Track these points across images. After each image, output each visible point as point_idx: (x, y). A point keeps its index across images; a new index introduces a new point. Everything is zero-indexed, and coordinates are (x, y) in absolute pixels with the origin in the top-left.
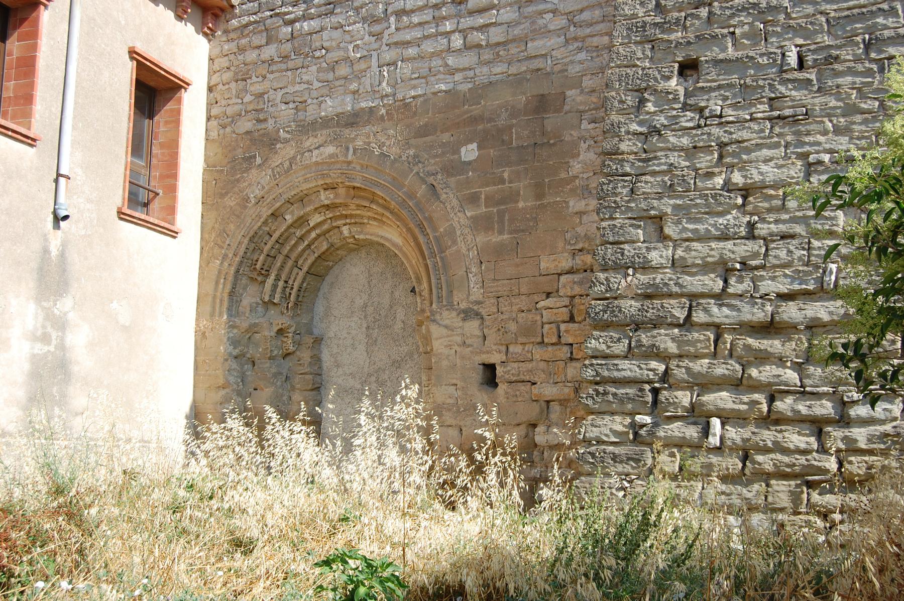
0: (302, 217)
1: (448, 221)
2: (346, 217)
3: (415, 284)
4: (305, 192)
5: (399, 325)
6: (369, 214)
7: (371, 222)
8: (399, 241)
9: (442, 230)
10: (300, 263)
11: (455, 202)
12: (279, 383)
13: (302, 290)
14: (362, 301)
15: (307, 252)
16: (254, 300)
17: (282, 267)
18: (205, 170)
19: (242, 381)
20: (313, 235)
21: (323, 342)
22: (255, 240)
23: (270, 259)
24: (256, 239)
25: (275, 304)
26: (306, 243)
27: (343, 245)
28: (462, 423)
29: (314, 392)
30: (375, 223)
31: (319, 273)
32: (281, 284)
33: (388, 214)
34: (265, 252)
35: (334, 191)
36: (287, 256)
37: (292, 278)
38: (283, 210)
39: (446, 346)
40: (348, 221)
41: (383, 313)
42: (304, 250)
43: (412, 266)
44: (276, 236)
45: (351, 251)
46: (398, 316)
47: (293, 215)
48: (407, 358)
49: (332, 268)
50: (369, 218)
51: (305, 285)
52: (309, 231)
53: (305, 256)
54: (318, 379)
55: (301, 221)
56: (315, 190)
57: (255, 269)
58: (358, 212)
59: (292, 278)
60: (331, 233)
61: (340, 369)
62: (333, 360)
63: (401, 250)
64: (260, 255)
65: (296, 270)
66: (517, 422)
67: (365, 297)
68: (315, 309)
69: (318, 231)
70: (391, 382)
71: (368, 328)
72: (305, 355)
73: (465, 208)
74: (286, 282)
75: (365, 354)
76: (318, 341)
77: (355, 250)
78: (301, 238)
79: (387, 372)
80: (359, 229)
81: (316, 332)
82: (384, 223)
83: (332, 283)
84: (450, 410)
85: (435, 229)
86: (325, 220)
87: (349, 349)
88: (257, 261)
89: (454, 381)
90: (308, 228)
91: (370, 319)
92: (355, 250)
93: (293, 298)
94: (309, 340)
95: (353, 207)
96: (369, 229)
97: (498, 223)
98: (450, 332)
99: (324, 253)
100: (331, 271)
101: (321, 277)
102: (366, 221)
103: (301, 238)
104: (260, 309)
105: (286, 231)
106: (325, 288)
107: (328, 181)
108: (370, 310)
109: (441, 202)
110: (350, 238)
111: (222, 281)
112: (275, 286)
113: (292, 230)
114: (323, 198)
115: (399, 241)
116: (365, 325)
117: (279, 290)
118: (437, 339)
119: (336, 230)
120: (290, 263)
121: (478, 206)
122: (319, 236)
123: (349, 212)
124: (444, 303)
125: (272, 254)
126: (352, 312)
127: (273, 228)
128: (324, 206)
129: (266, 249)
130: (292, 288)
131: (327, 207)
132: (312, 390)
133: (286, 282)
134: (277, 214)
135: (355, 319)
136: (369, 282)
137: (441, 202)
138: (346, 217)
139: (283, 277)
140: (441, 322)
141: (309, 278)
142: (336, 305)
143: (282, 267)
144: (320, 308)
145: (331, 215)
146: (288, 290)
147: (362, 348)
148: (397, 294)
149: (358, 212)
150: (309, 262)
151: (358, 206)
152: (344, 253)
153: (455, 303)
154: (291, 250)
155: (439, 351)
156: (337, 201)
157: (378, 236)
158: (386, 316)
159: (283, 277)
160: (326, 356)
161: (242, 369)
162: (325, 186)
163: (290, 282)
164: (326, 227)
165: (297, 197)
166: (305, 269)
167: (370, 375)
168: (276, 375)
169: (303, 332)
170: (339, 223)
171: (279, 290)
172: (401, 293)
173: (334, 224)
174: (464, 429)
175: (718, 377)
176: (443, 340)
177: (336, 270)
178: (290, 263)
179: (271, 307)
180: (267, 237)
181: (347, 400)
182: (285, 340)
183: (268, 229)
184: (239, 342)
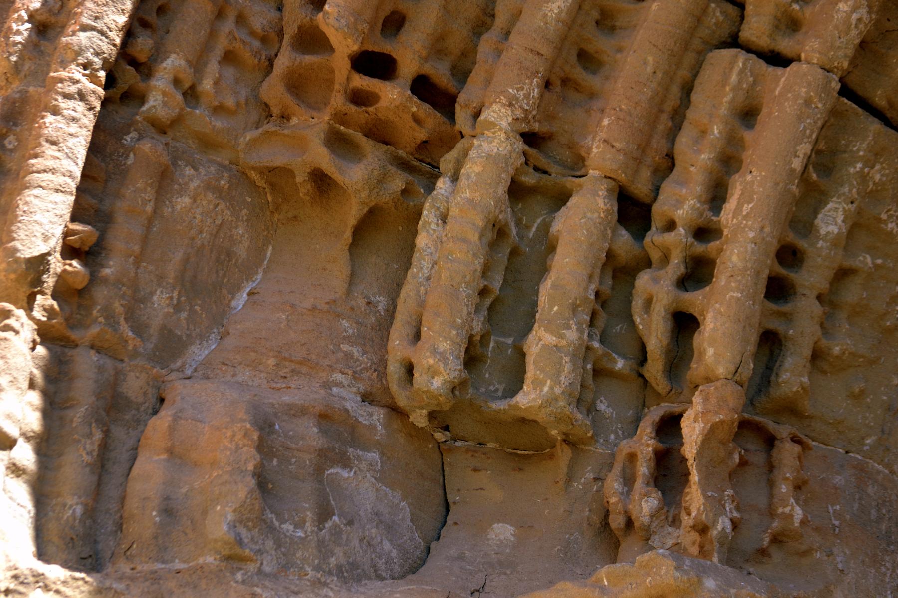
13: (811, 279)
32: (582, 222)
37: (697, 158)
51: (831, 221)
59: (697, 158)
74: (633, 212)
104: (363, 485)
117: (568, 275)
130: (698, 273)
139: (604, 144)
146: (656, 290)
159: (604, 144)
163: (681, 202)
171: (568, 275)
179: (481, 486)
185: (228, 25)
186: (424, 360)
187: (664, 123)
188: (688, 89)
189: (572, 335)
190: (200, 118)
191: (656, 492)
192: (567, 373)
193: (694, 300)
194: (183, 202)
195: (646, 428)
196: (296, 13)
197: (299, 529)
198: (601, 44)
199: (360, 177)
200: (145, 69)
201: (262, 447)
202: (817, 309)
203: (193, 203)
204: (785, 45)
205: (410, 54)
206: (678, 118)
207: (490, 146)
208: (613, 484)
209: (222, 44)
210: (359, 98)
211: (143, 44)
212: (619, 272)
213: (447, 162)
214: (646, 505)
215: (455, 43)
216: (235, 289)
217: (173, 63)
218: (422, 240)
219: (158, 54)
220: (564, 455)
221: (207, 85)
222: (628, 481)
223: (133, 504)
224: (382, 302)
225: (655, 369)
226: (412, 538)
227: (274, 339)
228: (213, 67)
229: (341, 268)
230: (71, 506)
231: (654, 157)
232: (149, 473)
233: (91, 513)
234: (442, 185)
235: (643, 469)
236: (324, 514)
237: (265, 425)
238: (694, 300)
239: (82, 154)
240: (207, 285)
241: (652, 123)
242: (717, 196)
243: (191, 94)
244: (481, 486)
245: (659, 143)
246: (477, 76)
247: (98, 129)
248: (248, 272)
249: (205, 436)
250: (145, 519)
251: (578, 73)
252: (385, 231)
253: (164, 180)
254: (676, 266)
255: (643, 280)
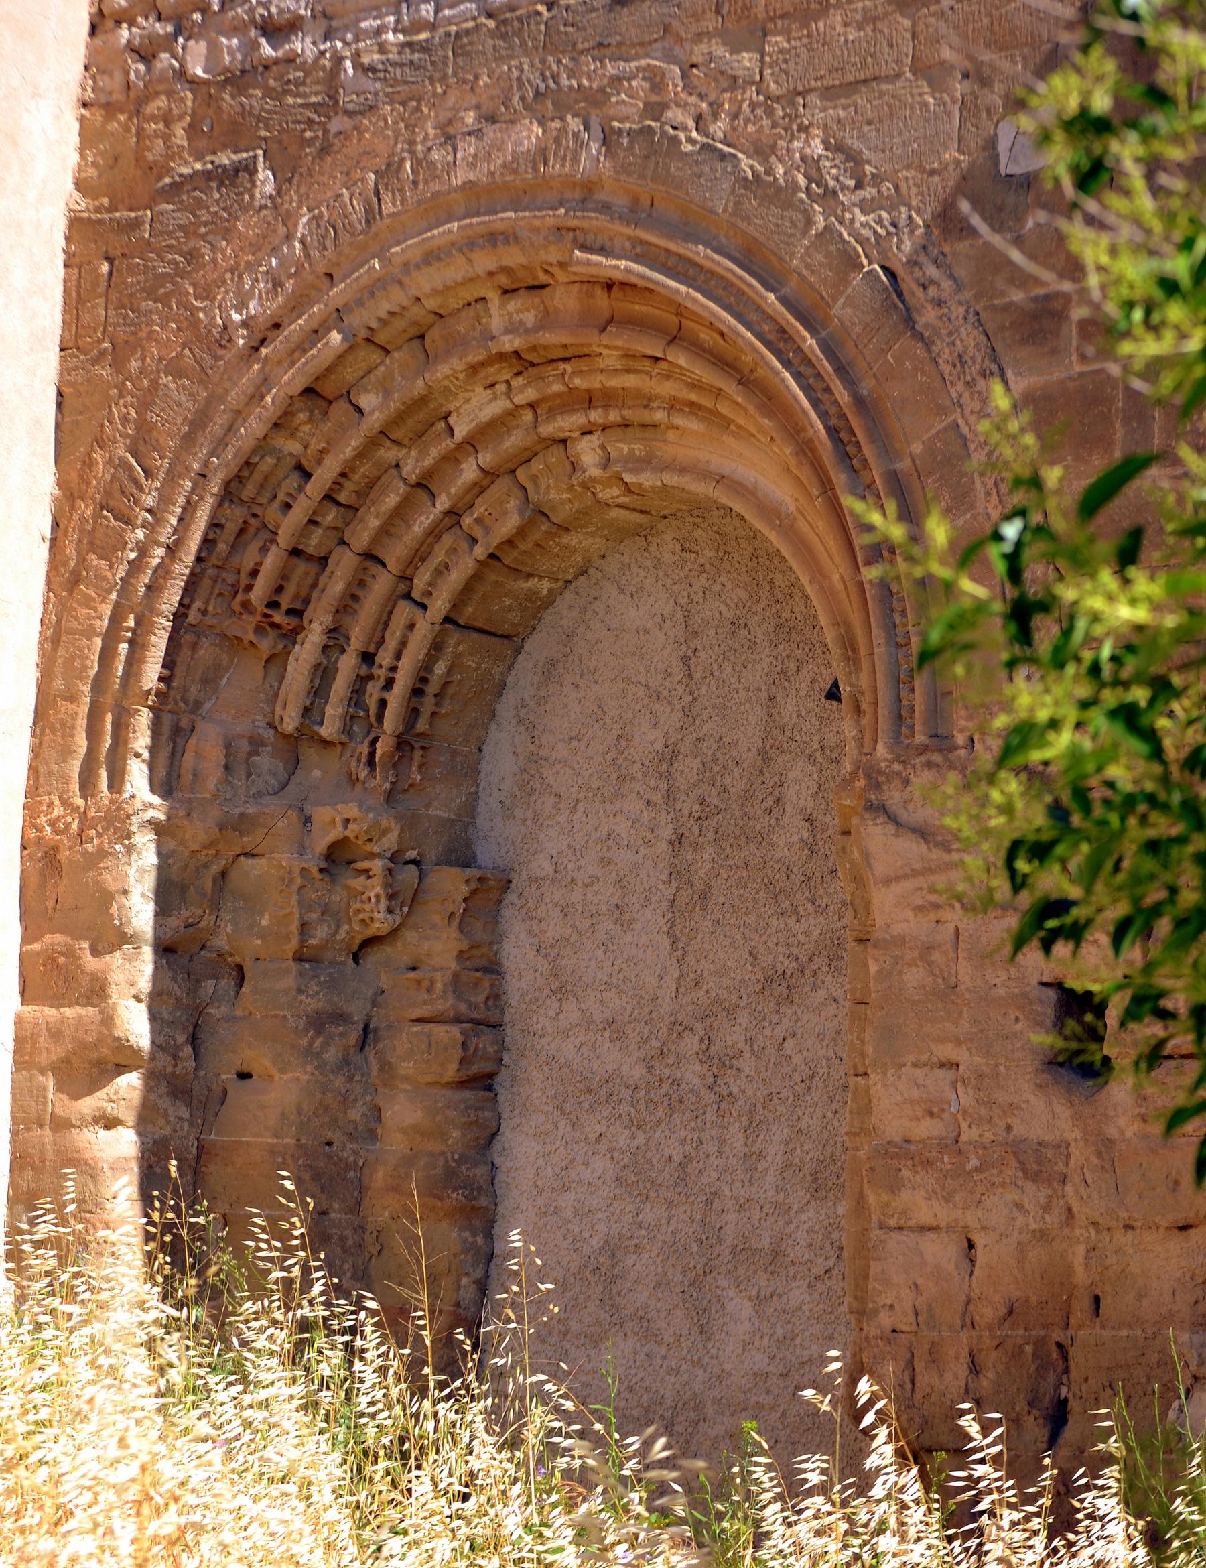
0: (423, 400)
1: (942, 411)
2: (589, 400)
3: (838, 670)
4: (431, 304)
5: (793, 831)
6: (668, 389)
7: (678, 421)
8: (783, 493)
9: (917, 448)
10: (421, 581)
11: (969, 337)
12: (332, 1054)
13: (431, 689)
14: (657, 735)
15: (447, 540)
16: (242, 727)
17: (349, 603)
18: (76, 224)
19: (194, 1040)
20: (469, 472)
21: (511, 897)
22: (244, 496)
23: (301, 567)
24: (248, 491)
25: (325, 744)
26: (443, 503)
27: (584, 512)
28: (971, 1218)
29: (468, 1094)
30: (694, 425)
31: (492, 628)
32: (347, 664)
33: (731, 388)
34: (284, 539)
35: (536, 298)
36: (371, 557)
37: (391, 644)
38: (349, 374)
39: (919, 909)
40: (595, 416)
41: (735, 782)
42: (434, 534)
43: (828, 593)
44: (324, 475)
45: (622, 534)
46: (790, 794)
47: (387, 393)
48: (819, 962)
49: (549, 601)
50: (673, 406)
51: (440, 668)
52: (452, 459)
53: (439, 555)
54: (485, 1042)
55: (422, 417)
56: (468, 294)
57: (246, 605)
58: (631, 381)
59: (391, 644)
60: (537, 466)
61: (570, 1006)
62: (544, 965)
63: (788, 529)
64: (264, 550)
65: (404, 611)
66: (1181, 1217)
67: (671, 718)
68: (484, 767)
69: (486, 458)
70: (757, 1056)
71: (678, 840)
72: (439, 946)
73: (1005, 360)
74: (368, 658)
75: (666, 943)
76: (490, 892)
77: (635, 532)
78: (424, 486)
79: (743, 1019)
80: (638, 448)
81: (486, 854)
82: (725, 424)
83: (552, 663)
84: (928, 1163)
85: (887, 447)
86: (513, 413)
87: (606, 926)
88: (254, 573)
89: (947, 1051)
90: (448, 444)
91: (687, 805)
92: (635, 532)
93: (391, 721)
94: (450, 885)
95: (611, 359)
96: (672, 448)
97: (1126, 421)
98: (936, 854)
99: (510, 542)
100: (548, 616)
101: (507, 639)
102: (659, 416)
103: (424, 486)
104: (266, 761)
105: (361, 455)
106: (523, 677)
107: (513, 257)
108: (687, 769)
109: (920, 337)
110: (607, 483)
111: (123, 647)
112: (323, 674)
113: (389, 454)
114: (496, 323)
115: (783, 493)
116: (667, 832)
117: (341, 686)
118: (888, 882)
119: (555, 456)
120: (381, 584)
121: (1054, 352)
122: (489, 475)
123: (596, 382)
124: (920, 739)
125: (314, 542)
126: (622, 778)
127: (316, 444)
128: (502, 356)
129: (289, 526)
130: (389, 684)
131: (520, 362)
132: (463, 1084)
133: (368, 658)
134: (328, 389)
135: (633, 805)
136: (685, 660)
137: (920, 337)
138: (589, 400)
139: (357, 638)
140: (903, 816)
141: (456, 642)
142: (562, 751)
143: (349, 603)
144: (501, 760)
145: (531, 394)
146: (373, 691)
147: (652, 919)
148: (788, 708)
149: (631, 381)
150: (455, 578)
151: (628, 356)
152: (594, 544)
153: (960, 739)
154: (385, 531)
155: (897, 929)
156: (550, 338)
157: (705, 475)
158: (747, 797)
159: (357, 638)
160: (518, 953)
161: (193, 992)
162: (503, 280)
163: (385, 658)
164: (514, 441)
165: (399, 324)
166: (439, 605)
167: (679, 1028)
168: (319, 1022)
169: (431, 855)
170: (566, 424)
171: (341, 686)
172: (799, 703)
173: (547, 430)
174: (979, 1240)
175: (125, 764)
176: (909, 884)
177: (565, 610)
178: (381, 584)
179: (310, 754)
180: (294, 480)
181: (593, 1128)
182: (359, 883)
183: (294, 447)
184: (184, 889)
185: (219, 585)
186: (286, 719)
187: (381, 626)
188: (391, 613)
189: (340, 710)
190: (209, 620)
191: (1123, 142)
192: (338, 724)
193: (386, 695)
194: (201, 652)
195: (366, 744)
196: (9, 1524)
197: (239, 782)
198: (360, 593)
199: (266, 645)
200: (188, 607)
201: (227, 756)
202: (433, 700)
203: (207, 651)
204: (426, 601)
205: (285, 601)
206: (386, 624)
207: (314, 636)
208: (354, 764)
209: (217, 591)
210: (266, 616)
211: (186, 601)
212: (361, 682)
213: (300, 638)
214: (363, 773)
215: (304, 592)
216: (221, 678)
217: (198, 604)
218: (289, 668)
219: (192, 601)
220: (339, 748)
221: (210, 608)
222: (359, 761)
223: (183, 771)
224: (276, 684)
225: (373, 719)
226: (283, 775)
227: (238, 703)
228: (213, 602)
229: (261, 674)
230: (162, 772)
231: (376, 639)
232: (188, 760)
233: (169, 773)
234: (297, 647)
235: (364, 760)
236: (249, 775)
237: (228, 746)
238: (386, 695)
239: (164, 648)
240: (209, 681)
241: (374, 630)
242: (398, 656)
243: (204, 612)
244: (310, 754)
245: (378, 634)
246: (311, 607)
247: (170, 638)
248: (227, 670)
249: (207, 749)
250: (187, 778)
251: (351, 603)
252: (276, 661)
253: (194, 646)
254: (382, 682)
255: (370, 686)
